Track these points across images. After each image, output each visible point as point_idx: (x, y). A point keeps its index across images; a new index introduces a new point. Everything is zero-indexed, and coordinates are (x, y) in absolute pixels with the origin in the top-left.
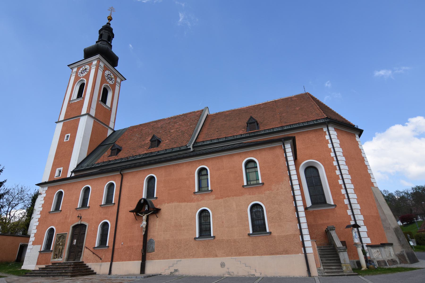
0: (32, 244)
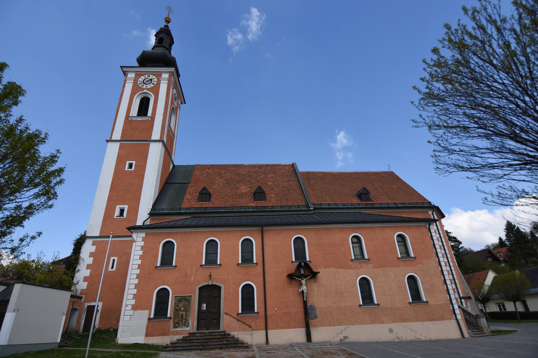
0: (132, 309)
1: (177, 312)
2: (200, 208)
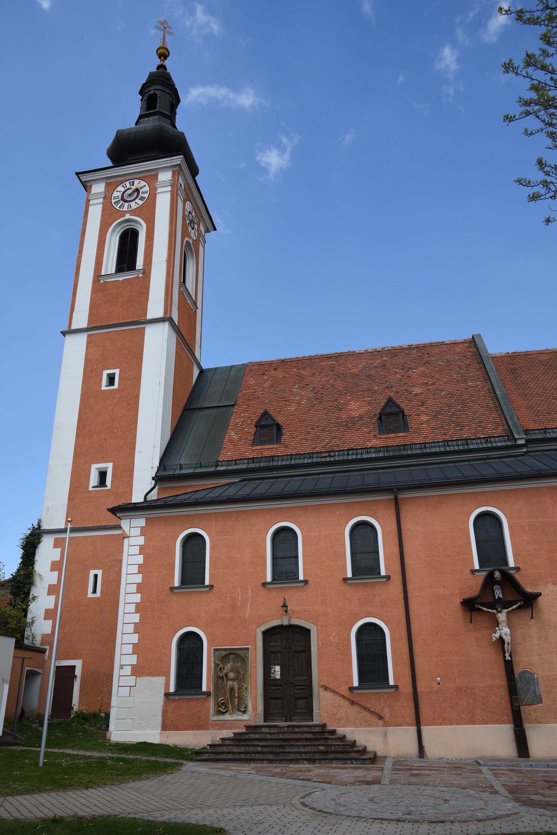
0: (133, 674)
1: (220, 682)
2: (259, 459)
